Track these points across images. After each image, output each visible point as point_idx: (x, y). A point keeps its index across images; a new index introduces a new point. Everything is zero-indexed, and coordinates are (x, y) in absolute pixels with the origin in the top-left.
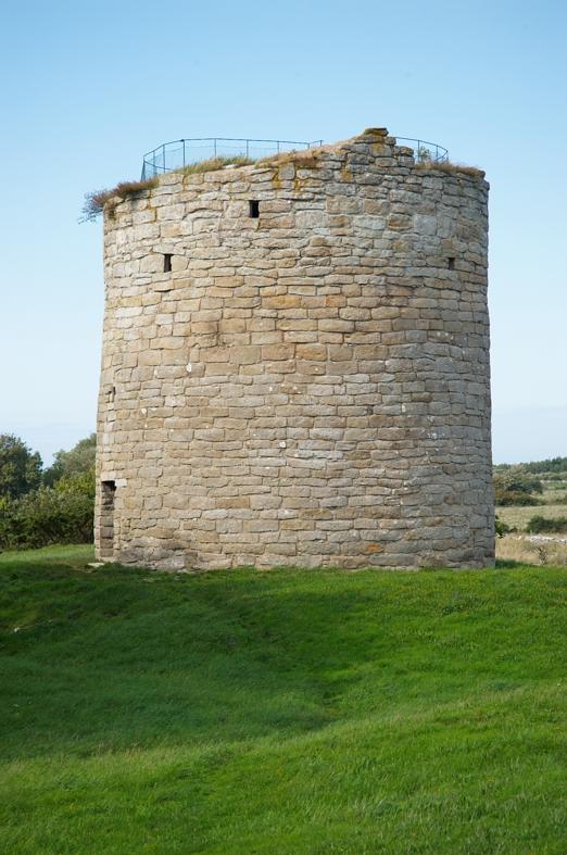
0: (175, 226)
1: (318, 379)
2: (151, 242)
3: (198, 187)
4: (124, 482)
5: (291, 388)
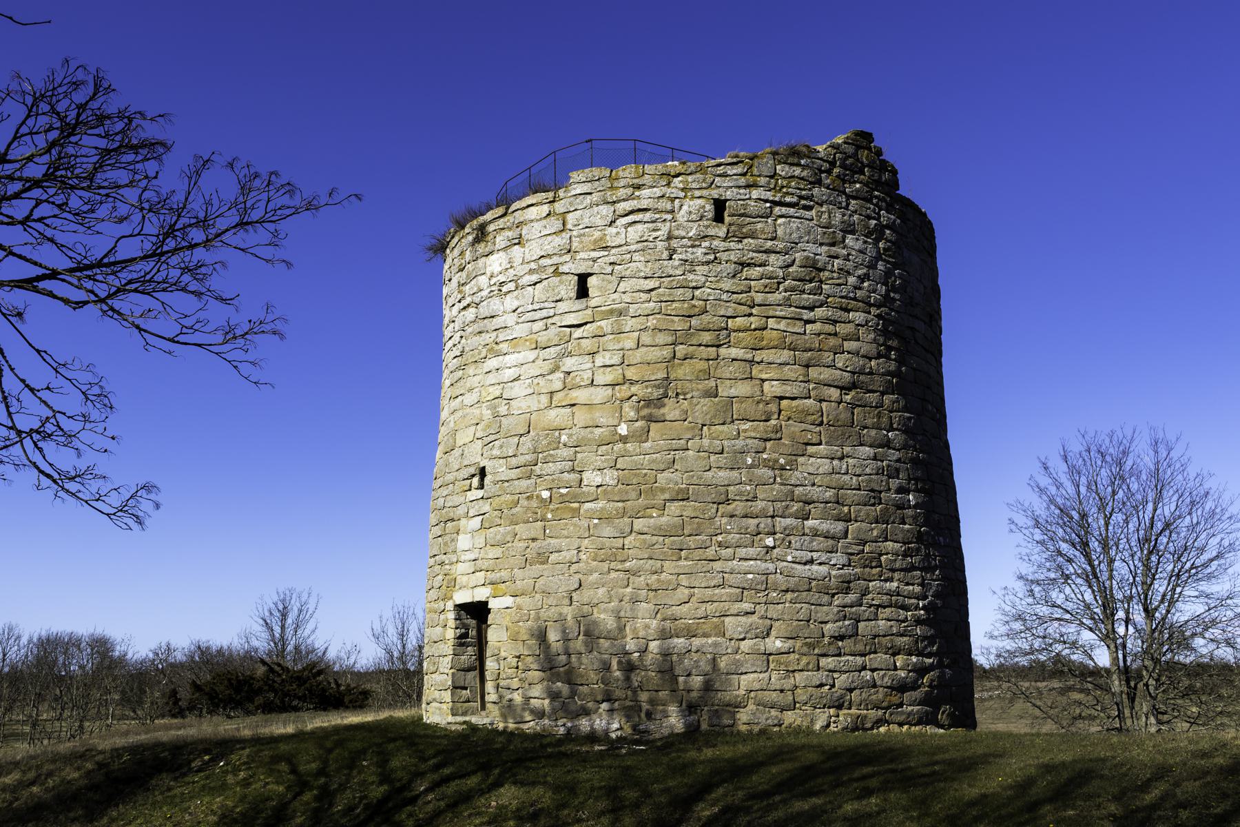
0: (597, 234)
1: (811, 449)
2: (556, 260)
3: (636, 181)
4: (508, 601)
5: (777, 461)
